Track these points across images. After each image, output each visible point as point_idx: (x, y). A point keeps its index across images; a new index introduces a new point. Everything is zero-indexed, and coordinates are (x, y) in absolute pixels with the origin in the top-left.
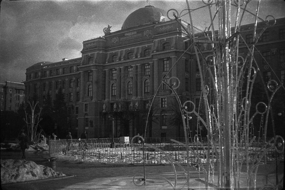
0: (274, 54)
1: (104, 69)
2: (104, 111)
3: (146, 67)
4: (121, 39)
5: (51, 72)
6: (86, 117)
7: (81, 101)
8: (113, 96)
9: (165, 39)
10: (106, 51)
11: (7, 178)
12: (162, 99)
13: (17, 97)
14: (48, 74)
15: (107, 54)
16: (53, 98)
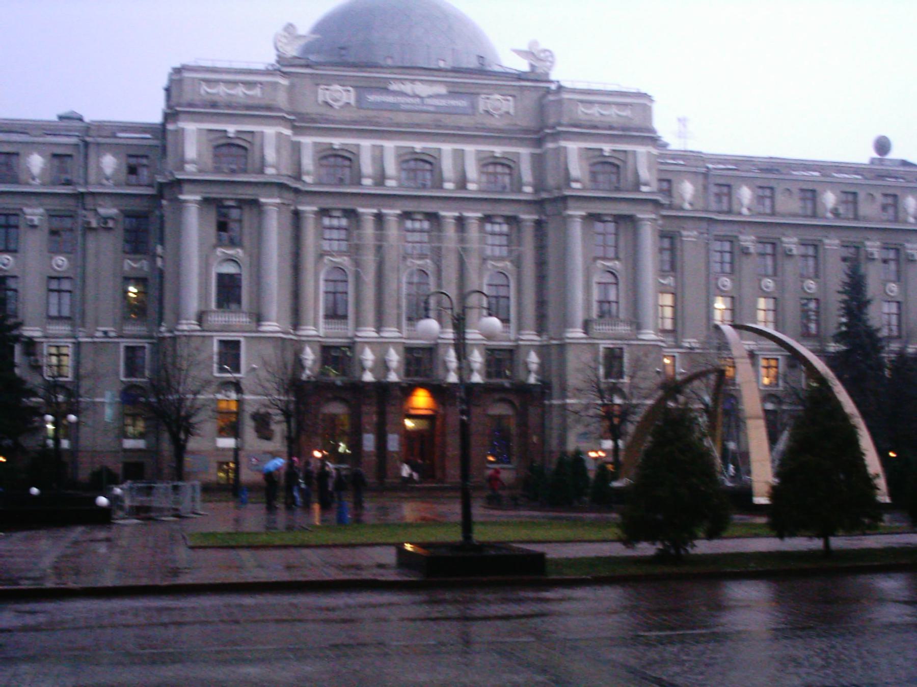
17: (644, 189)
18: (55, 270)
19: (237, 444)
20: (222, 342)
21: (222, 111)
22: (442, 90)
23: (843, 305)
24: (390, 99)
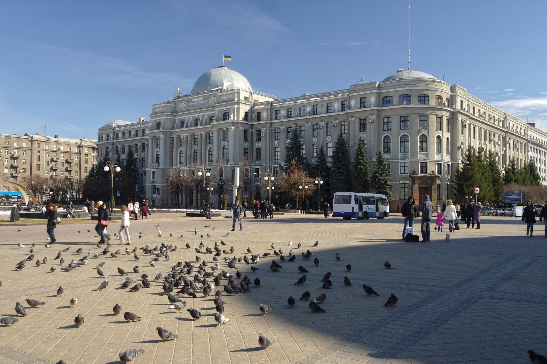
0: (336, 126)
3: (210, 135)
5: (124, 134)
8: (181, 163)
9: (225, 108)
10: (175, 116)
11: (45, 214)
12: (274, 168)
13: (95, 158)
14: (120, 137)
15: (175, 120)
16: (330, 152)
24: (193, 103)
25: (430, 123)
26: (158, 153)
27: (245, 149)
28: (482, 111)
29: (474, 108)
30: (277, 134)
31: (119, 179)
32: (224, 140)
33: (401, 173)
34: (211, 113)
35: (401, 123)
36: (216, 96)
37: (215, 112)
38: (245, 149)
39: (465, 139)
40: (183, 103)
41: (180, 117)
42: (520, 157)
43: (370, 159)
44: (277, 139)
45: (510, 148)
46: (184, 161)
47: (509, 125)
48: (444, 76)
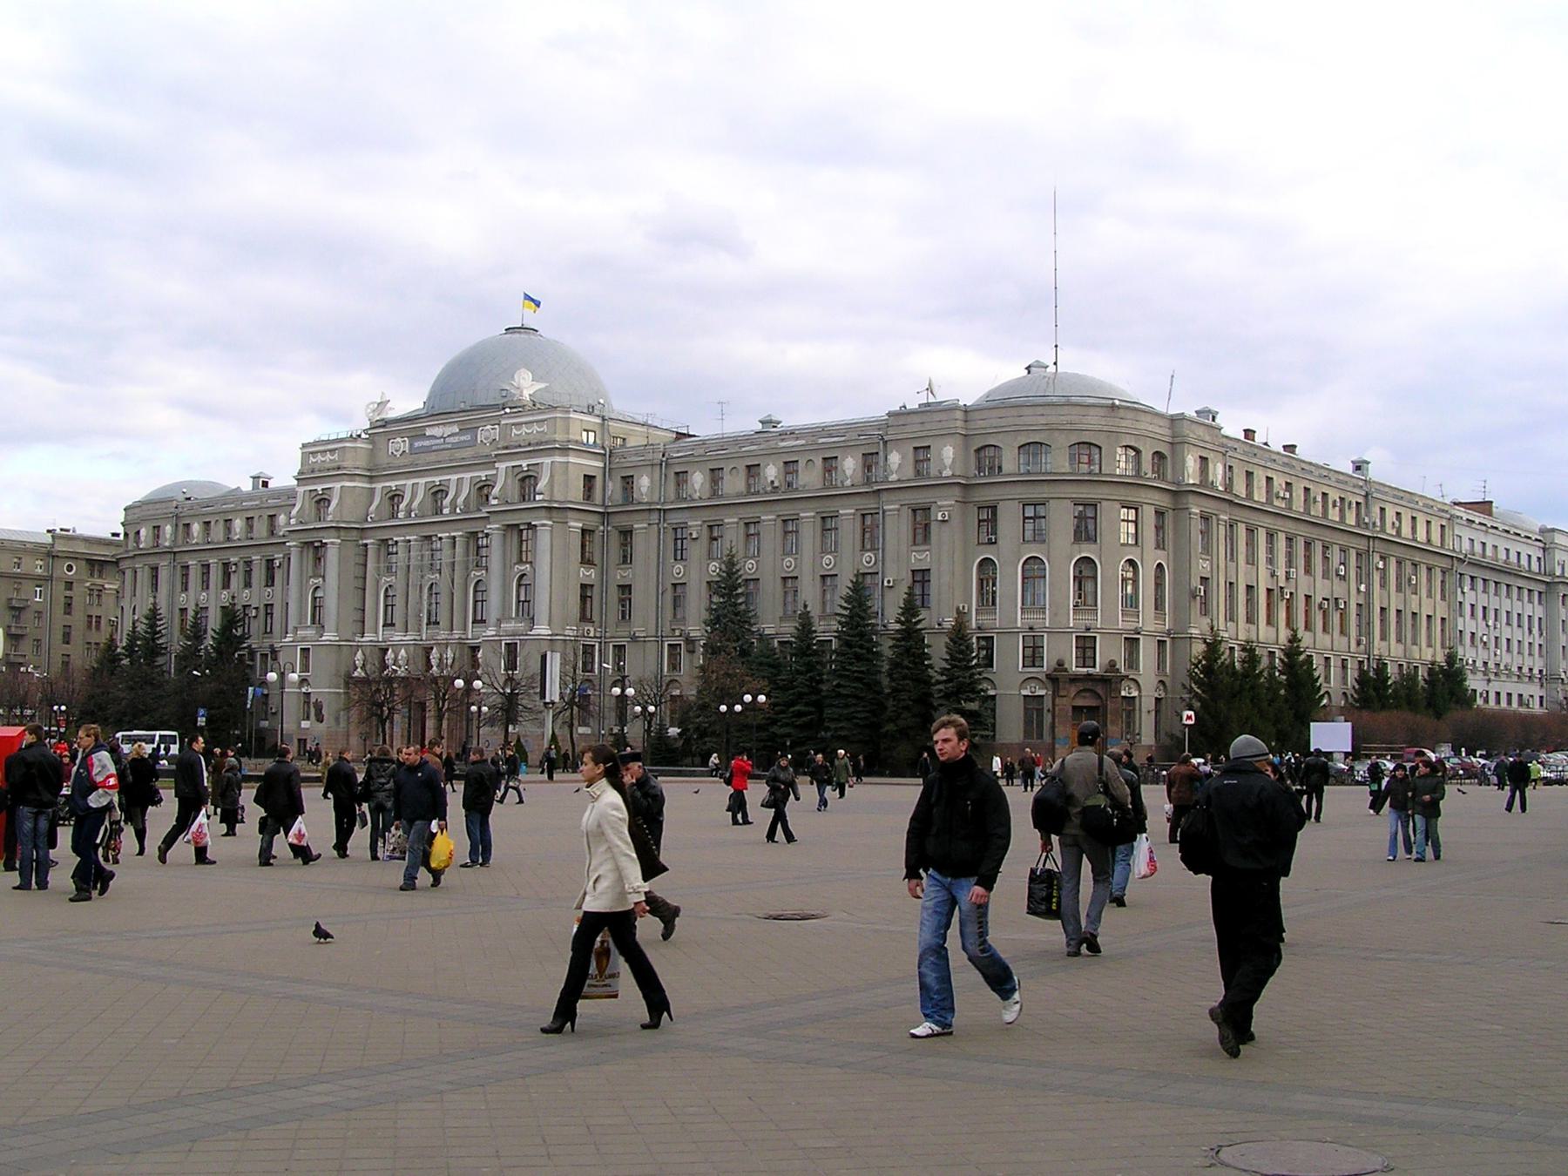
1: (362, 539)
2: (359, 673)
4: (416, 444)
6: (304, 690)
7: (291, 639)
15: (372, 490)
17: (538, 497)
18: (786, 572)
19: (272, 683)
20: (779, 642)
21: (308, 476)
22: (456, 429)
23: (827, 629)
24: (427, 443)
25: (1104, 524)
26: (319, 594)
27: (584, 587)
28: (1279, 482)
29: (1249, 474)
30: (679, 542)
31: (203, 673)
32: (520, 561)
33: (1024, 666)
34: (483, 474)
35: (1024, 522)
36: (499, 424)
37: (494, 472)
38: (584, 587)
39: (1215, 567)
40: (399, 440)
41: (387, 484)
42: (1425, 611)
43: (939, 625)
44: (679, 558)
45: (1383, 585)
46: (398, 620)
47: (1383, 518)
48: (1172, 376)
